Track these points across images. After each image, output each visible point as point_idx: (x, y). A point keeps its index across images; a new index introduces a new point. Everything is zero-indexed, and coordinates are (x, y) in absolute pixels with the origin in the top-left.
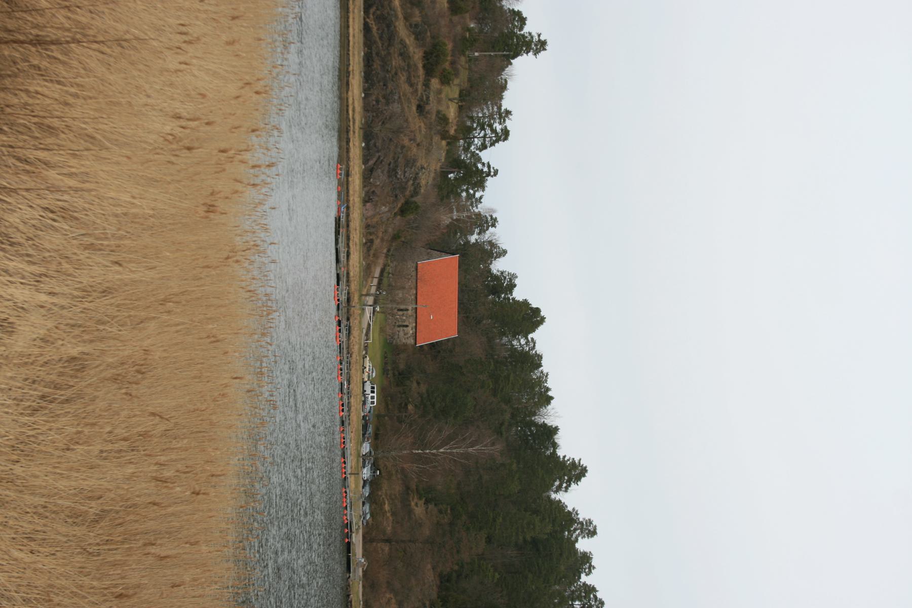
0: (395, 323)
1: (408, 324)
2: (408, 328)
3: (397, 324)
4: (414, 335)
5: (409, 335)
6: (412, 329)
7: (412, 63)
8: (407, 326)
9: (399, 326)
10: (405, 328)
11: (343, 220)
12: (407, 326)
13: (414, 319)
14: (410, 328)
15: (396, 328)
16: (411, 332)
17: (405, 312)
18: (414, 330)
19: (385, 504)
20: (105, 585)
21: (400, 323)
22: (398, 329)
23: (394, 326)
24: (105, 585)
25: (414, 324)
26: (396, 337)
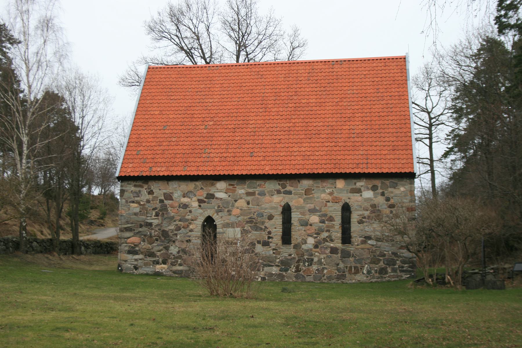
0: (334, 251)
1: (338, 207)
2: (354, 206)
3: (338, 245)
4: (378, 182)
5: (380, 200)
6: (358, 191)
7: (105, 244)
8: (346, 209)
9: (346, 238)
10: (355, 217)
11: (192, 60)
12: (346, 209)
13: (319, 183)
14: (354, 200)
15: (351, 248)
16: (368, 194)
17: (295, 216)
18: (360, 184)
19: (453, 283)
20: (145, 271)
21: (337, 234)
22: (356, 239)
23: (346, 255)
24: (145, 271)
25: (340, 184)
26: (387, 248)
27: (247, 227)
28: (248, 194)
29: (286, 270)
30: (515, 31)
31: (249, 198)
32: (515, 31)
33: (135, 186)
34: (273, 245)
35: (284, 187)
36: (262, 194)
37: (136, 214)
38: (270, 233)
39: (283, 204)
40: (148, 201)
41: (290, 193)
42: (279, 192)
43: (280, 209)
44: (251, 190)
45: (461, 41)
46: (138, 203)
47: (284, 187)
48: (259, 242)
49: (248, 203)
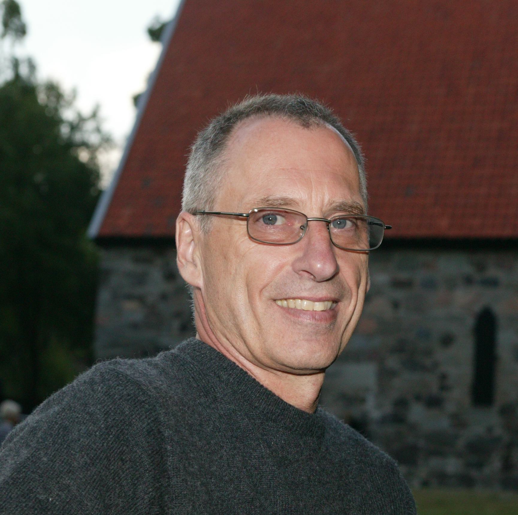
27: (393, 362)
28: (398, 284)
29: (480, 465)
30: (231, 248)
31: (399, 295)
32: (231, 248)
33: (137, 260)
34: (450, 407)
35: (481, 268)
36: (430, 285)
37: (135, 326)
38: (444, 377)
39: (477, 308)
40: (164, 297)
41: (493, 283)
42: (469, 281)
43: (470, 322)
44: (403, 276)
45: (270, 299)
46: (141, 299)
47: (481, 268)
48: (418, 398)
49: (396, 305)
